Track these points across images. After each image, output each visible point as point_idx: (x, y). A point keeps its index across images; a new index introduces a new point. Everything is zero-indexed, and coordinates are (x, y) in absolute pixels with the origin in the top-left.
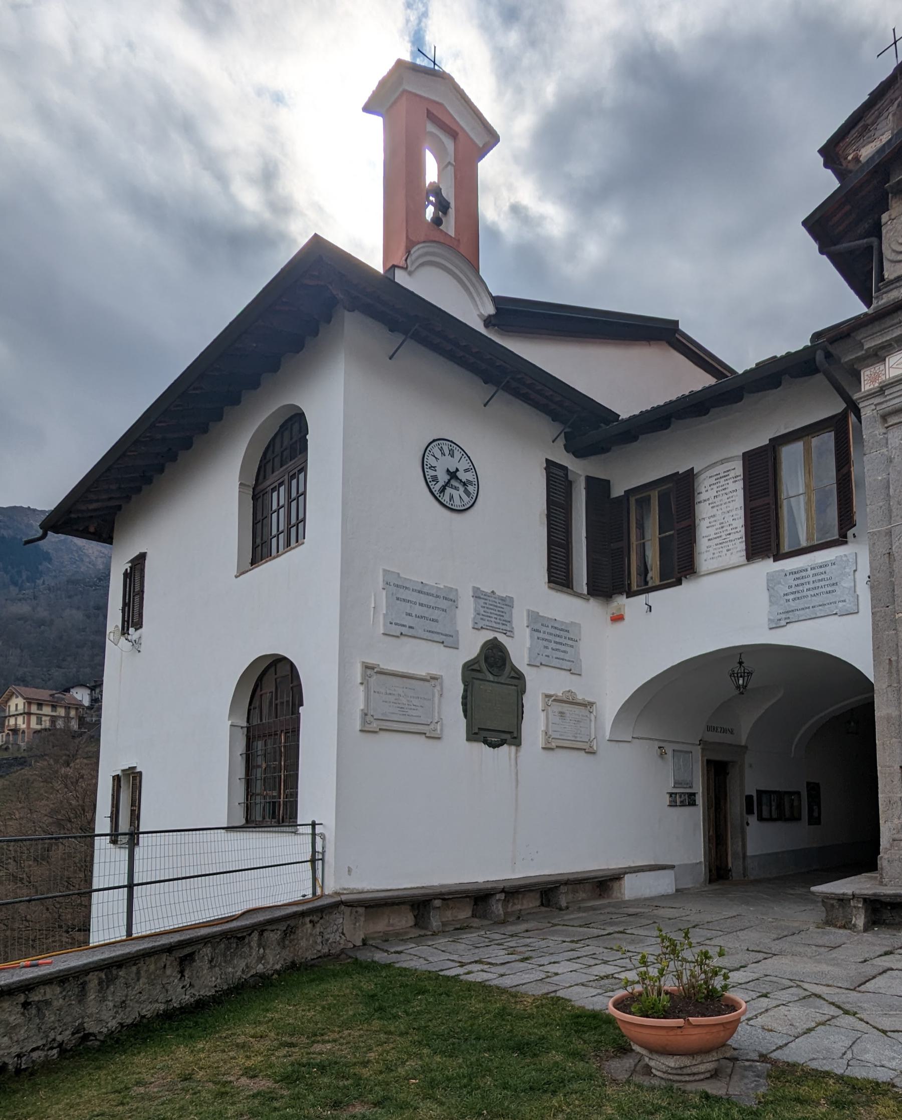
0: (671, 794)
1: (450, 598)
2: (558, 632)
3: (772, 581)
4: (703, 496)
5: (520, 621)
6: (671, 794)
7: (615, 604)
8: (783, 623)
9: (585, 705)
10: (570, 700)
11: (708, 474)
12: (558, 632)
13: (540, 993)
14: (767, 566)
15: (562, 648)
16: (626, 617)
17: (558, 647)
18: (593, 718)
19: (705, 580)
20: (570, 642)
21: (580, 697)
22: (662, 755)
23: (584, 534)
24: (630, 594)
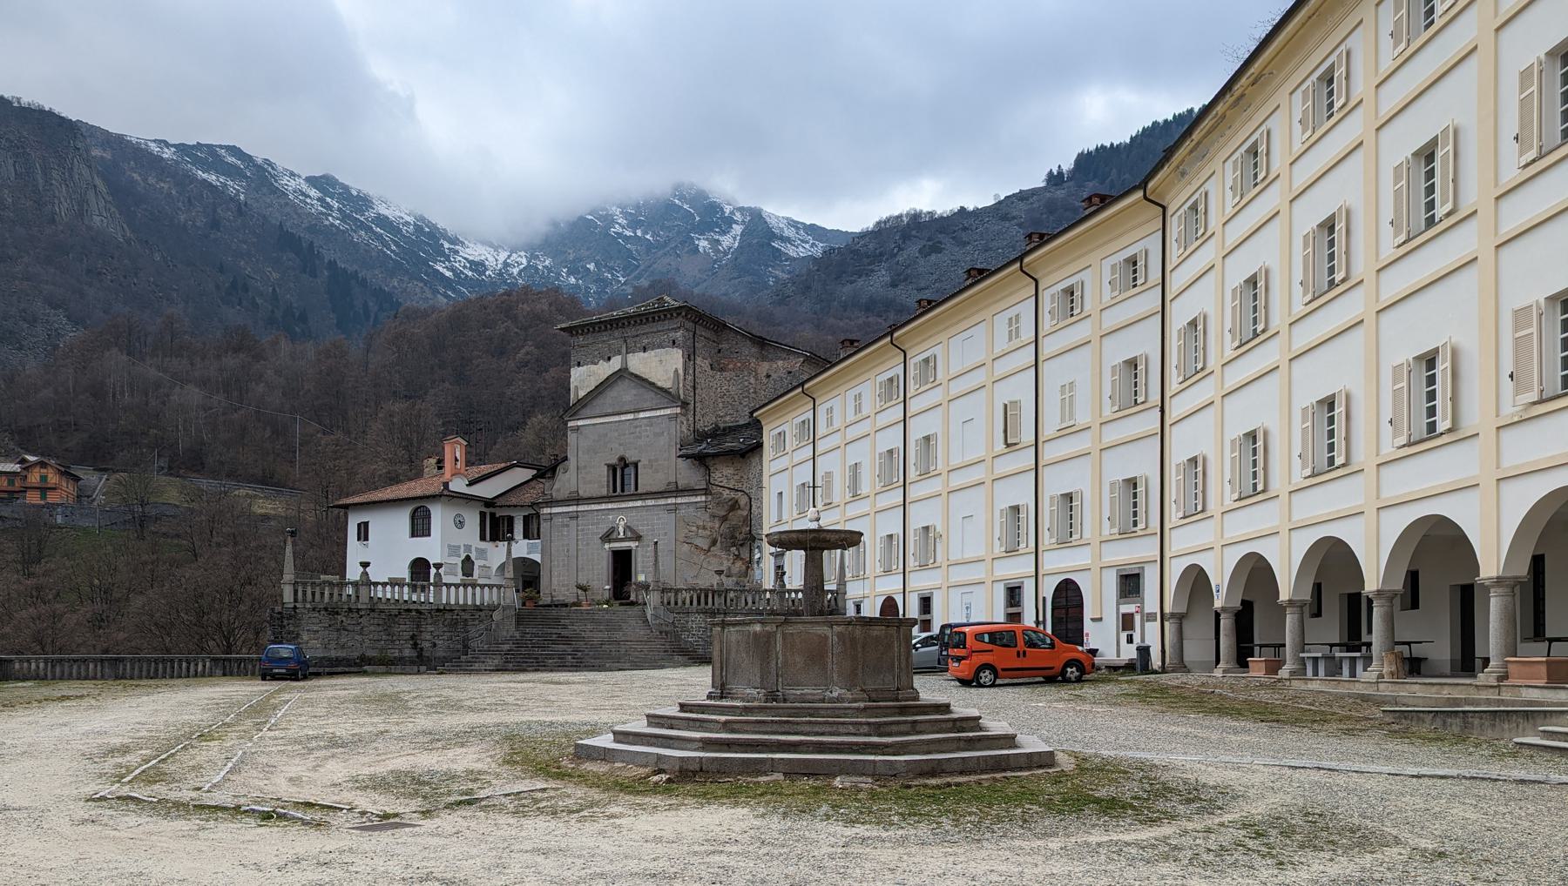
1: (459, 547)
5: (473, 549)
10: (485, 566)
14: (527, 541)
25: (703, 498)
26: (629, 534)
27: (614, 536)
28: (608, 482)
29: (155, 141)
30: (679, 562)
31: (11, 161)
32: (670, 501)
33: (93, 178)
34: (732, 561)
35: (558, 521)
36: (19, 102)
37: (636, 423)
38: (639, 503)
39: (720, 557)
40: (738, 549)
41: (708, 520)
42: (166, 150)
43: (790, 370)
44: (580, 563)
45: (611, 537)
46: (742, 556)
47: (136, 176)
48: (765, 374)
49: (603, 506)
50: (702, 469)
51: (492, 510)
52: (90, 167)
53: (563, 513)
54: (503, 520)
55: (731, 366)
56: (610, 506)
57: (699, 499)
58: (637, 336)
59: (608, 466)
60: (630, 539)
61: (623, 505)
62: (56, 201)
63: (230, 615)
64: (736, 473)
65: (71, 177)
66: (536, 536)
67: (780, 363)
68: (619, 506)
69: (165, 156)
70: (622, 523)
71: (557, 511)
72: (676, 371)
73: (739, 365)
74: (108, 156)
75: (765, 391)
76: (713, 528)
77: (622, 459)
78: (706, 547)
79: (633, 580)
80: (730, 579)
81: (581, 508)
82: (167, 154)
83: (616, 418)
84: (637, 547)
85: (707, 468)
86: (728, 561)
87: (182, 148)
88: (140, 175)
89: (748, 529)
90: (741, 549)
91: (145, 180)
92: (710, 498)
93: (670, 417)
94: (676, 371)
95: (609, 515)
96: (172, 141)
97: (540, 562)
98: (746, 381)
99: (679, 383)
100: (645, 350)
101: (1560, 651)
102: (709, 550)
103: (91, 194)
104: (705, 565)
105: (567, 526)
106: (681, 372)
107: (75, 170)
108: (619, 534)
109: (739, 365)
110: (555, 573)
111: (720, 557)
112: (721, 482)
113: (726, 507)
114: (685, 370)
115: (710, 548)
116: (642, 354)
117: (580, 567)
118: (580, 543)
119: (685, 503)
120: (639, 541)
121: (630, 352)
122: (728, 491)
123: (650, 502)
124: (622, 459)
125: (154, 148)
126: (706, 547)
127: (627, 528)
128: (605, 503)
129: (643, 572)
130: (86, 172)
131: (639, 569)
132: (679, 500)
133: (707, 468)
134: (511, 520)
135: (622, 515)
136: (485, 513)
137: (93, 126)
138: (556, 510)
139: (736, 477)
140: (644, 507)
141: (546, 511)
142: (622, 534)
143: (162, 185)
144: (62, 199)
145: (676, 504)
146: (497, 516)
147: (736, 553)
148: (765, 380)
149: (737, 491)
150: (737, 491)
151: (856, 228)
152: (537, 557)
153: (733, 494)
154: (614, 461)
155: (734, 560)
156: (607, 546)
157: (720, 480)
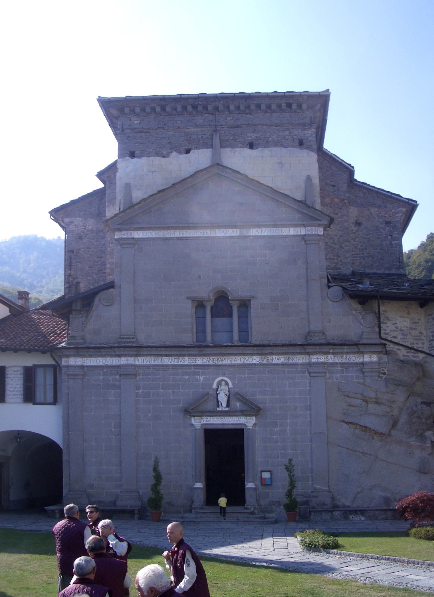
4: (9, 376)
25: (375, 358)
26: (237, 405)
38: (256, 360)
43: (387, 220)
48: (353, 220)
49: (186, 361)
56: (199, 361)
57: (367, 358)
58: (237, 127)
59: (193, 300)
60: (243, 413)
61: (225, 361)
63: (236, 421)
64: (414, 326)
66: (50, 397)
68: (216, 362)
71: (92, 364)
72: (309, 179)
73: (336, 200)
75: (354, 240)
81: (141, 361)
94: (309, 179)
95: (198, 374)
100: (251, 146)
106: (316, 181)
112: (395, 337)
121: (226, 147)
123: (275, 359)
126: (383, 430)
128: (189, 355)
135: (224, 375)
140: (264, 365)
148: (354, 228)
149: (417, 351)
150: (417, 351)
151: (118, 143)
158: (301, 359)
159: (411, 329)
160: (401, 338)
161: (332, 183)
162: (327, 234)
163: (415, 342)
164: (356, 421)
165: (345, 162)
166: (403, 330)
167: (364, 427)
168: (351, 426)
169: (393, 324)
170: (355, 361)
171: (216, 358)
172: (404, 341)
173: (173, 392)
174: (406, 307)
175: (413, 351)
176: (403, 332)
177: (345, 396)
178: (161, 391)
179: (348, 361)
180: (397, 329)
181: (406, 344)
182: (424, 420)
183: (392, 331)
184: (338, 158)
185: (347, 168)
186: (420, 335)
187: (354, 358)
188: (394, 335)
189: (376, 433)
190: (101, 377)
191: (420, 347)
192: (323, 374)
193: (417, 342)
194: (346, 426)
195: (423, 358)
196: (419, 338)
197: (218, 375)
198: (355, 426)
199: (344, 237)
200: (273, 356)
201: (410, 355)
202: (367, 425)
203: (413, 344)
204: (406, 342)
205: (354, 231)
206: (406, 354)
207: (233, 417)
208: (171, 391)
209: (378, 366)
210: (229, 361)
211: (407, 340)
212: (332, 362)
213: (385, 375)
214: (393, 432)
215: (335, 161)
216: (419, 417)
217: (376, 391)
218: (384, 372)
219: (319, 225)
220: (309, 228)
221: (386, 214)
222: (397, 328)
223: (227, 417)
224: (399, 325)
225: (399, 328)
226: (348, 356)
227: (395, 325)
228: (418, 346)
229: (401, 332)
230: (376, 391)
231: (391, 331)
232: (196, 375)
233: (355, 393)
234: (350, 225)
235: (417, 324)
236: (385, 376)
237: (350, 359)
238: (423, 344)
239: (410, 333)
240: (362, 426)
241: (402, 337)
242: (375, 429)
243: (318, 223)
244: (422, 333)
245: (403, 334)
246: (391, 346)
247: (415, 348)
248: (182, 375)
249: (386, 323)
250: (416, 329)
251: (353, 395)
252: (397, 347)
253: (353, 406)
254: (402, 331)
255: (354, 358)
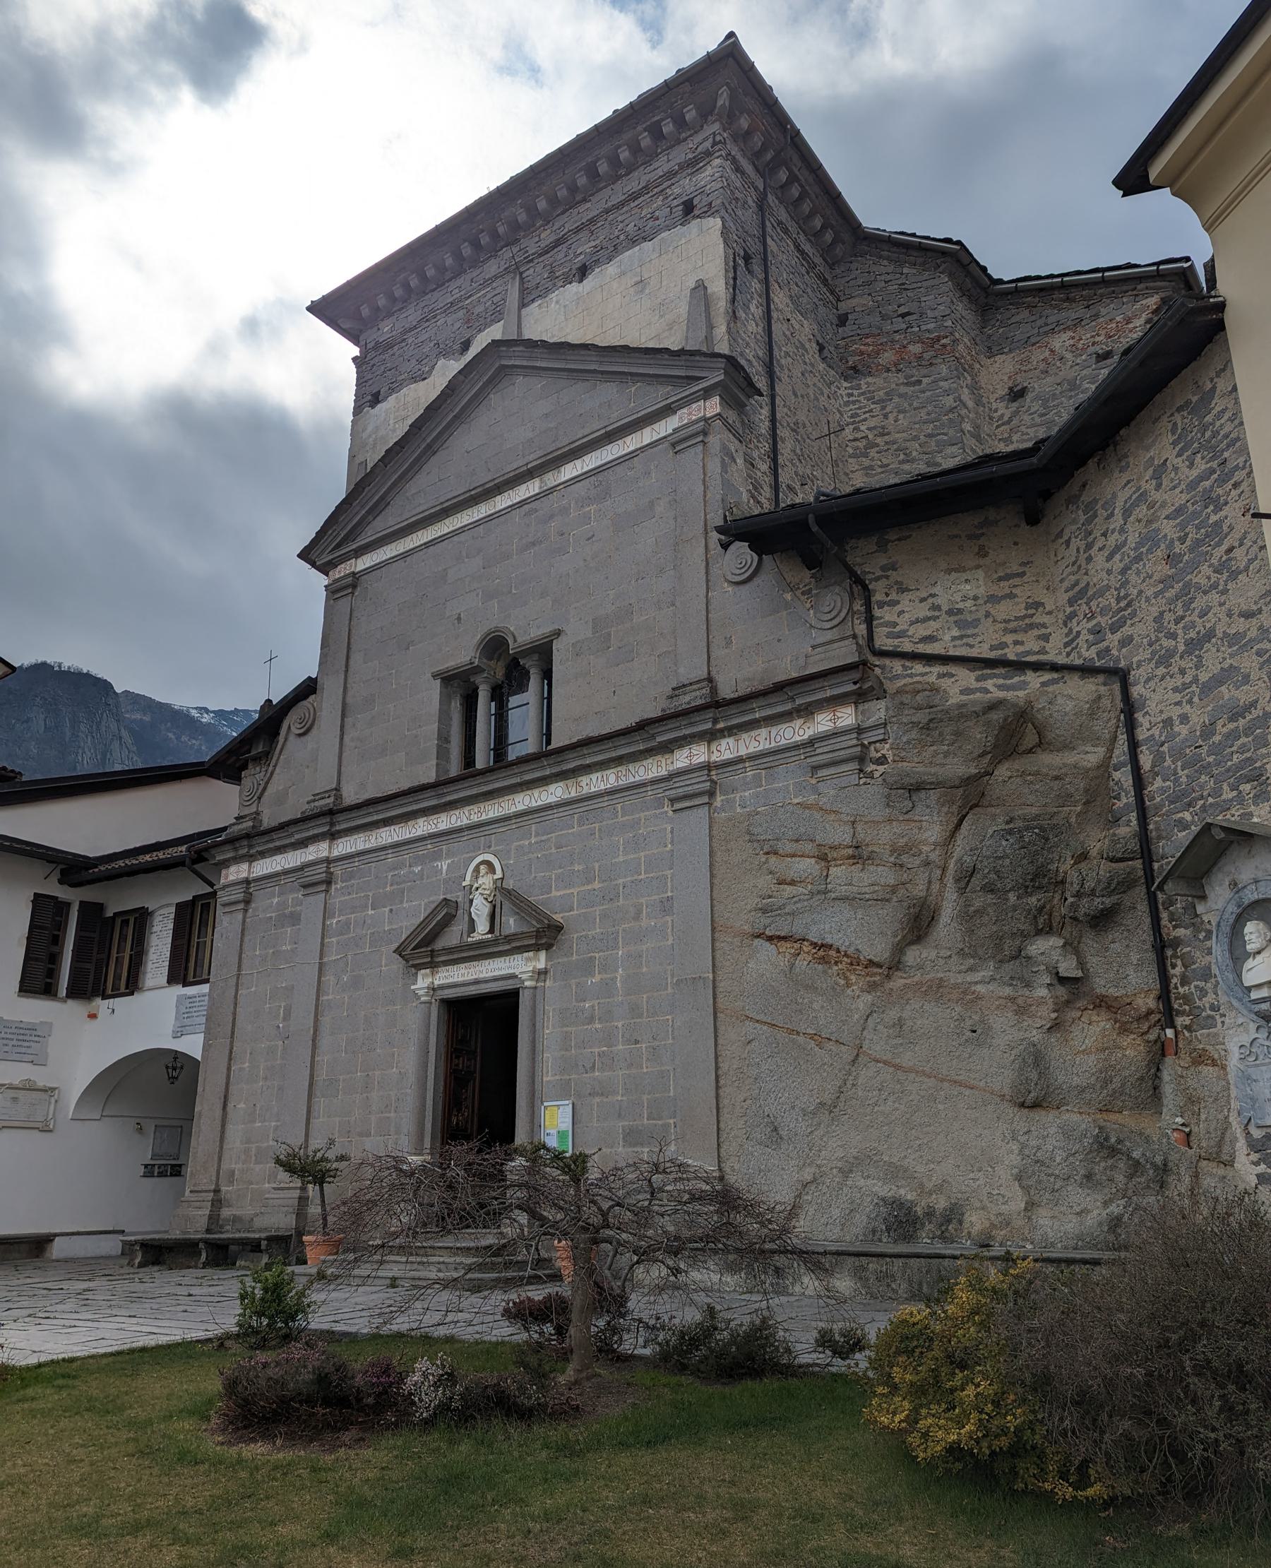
0: (146, 1166)
2: (22, 1031)
3: (180, 1000)
4: (154, 929)
6: (146, 1166)
7: (94, 1004)
8: (179, 1034)
9: (45, 1090)
11: (161, 912)
12: (22, 1031)
13: (23, 1363)
14: (179, 990)
15: (26, 1044)
16: (100, 1016)
17: (20, 1043)
18: (53, 1100)
19: (147, 993)
20: (36, 1039)
21: (40, 1084)
22: (140, 1130)
23: (71, 948)
24: (105, 997)
25: (846, 717)
26: (511, 924)
27: (452, 937)
28: (444, 738)
29: (196, 708)
30: (732, 1034)
31: (42, 717)
32: (682, 759)
33: (119, 730)
34: (1046, 1014)
35: (268, 903)
36: (60, 667)
37: (554, 501)
38: (555, 792)
39: (969, 998)
40: (1072, 947)
41: (879, 813)
42: (206, 715)
43: (1099, 349)
44: (323, 1058)
45: (440, 944)
46: (1102, 984)
47: (171, 735)
48: (1002, 391)
49: (422, 827)
50: (835, 599)
51: (89, 894)
52: (118, 721)
53: (286, 872)
54: (126, 922)
55: (888, 357)
56: (444, 822)
57: (823, 723)
61: (492, 810)
62: (80, 751)
65: (98, 729)
67: (1060, 342)
68: (475, 818)
69: (204, 720)
70: (486, 881)
72: (701, 286)
73: (916, 349)
74: (147, 718)
76: (909, 848)
77: (495, 645)
78: (878, 949)
79: (521, 1137)
80: (1049, 1121)
82: (206, 719)
83: (482, 511)
84: (542, 974)
85: (860, 586)
86: (1022, 1011)
87: (220, 714)
88: (174, 734)
89: (1128, 829)
90: (1090, 943)
91: (178, 738)
92: (878, 710)
93: (677, 443)
95: (437, 856)
96: (211, 708)
97: (198, 1055)
98: (947, 393)
99: (711, 327)
101: (14, 1073)
102: (895, 965)
103: (116, 744)
104: (877, 1044)
105: (295, 919)
106: (718, 287)
107: (103, 723)
108: (472, 927)
109: (916, 349)
110: (239, 1106)
111: (969, 998)
113: (979, 736)
114: (734, 286)
115: (899, 950)
116: (574, 288)
117: (322, 1075)
118: (329, 978)
119: (752, 757)
120: (548, 947)
122: (966, 677)
123: (595, 783)
124: (495, 645)
125: (194, 713)
126: (878, 949)
127: (505, 897)
129: (564, 1091)
130: (113, 726)
131: (549, 1076)
132: (726, 749)
133: (860, 586)
134: (142, 918)
136: (61, 908)
137: (138, 695)
138: (264, 867)
139: (1003, 610)
141: (237, 872)
142: (482, 927)
143: (194, 742)
144: (86, 750)
145: (708, 767)
146: (109, 914)
147: (1068, 967)
148: (1004, 410)
152: (192, 1045)
153: (994, 687)
154: (463, 653)
155: (1061, 1007)
156: (423, 981)
157: (922, 631)
158: (654, 769)
159: (993, 599)
160: (954, 639)
161: (903, 310)
162: (887, 443)
163: (1009, 639)
164: (798, 928)
165: (934, 239)
166: (960, 611)
167: (822, 945)
168: (784, 946)
169: (923, 600)
170: (793, 740)
171: (475, 808)
172: (967, 645)
173: (391, 911)
174: (970, 537)
175: (1002, 671)
176: (962, 617)
177: (767, 853)
178: (370, 912)
179: (773, 744)
180: (937, 613)
181: (973, 653)
182: (1012, 897)
183: (917, 621)
184: (913, 235)
185: (944, 253)
186: (1031, 612)
187: (795, 732)
188: (928, 633)
189: (855, 962)
190: (276, 900)
191: (1028, 653)
192: (705, 799)
193: (1019, 637)
194: (768, 949)
195: (1043, 684)
196: (1027, 621)
197: (477, 850)
198: (797, 945)
199: (939, 434)
200: (591, 776)
201: (989, 684)
202: (829, 941)
203: (1003, 645)
204: (972, 646)
205: (1006, 418)
206: (975, 685)
207: (499, 959)
208: (387, 910)
209: (858, 739)
210: (501, 809)
211: (979, 639)
212: (732, 756)
213: (882, 764)
214: (913, 955)
215: (904, 251)
216: (989, 889)
217: (853, 823)
218: (879, 754)
219: (706, 394)
220: (685, 410)
221: (1098, 335)
222: (936, 608)
223: (487, 962)
224: (942, 601)
225: (945, 608)
226: (774, 730)
227: (930, 600)
228: (1020, 649)
229: (952, 619)
230: (853, 823)
231: (912, 623)
232: (436, 860)
233: (797, 841)
234: (994, 406)
235: (1017, 581)
236: (881, 769)
237: (777, 740)
238: (1046, 638)
239: (988, 615)
240: (814, 945)
241: (955, 632)
242: (851, 951)
243: (701, 387)
244: (1038, 605)
245: (960, 624)
246: (913, 671)
247: (1012, 657)
248: (410, 866)
249: (894, 603)
250: (1011, 596)
251: (789, 847)
252: (937, 669)
253: (792, 883)
254: (956, 614)
255: (789, 733)
